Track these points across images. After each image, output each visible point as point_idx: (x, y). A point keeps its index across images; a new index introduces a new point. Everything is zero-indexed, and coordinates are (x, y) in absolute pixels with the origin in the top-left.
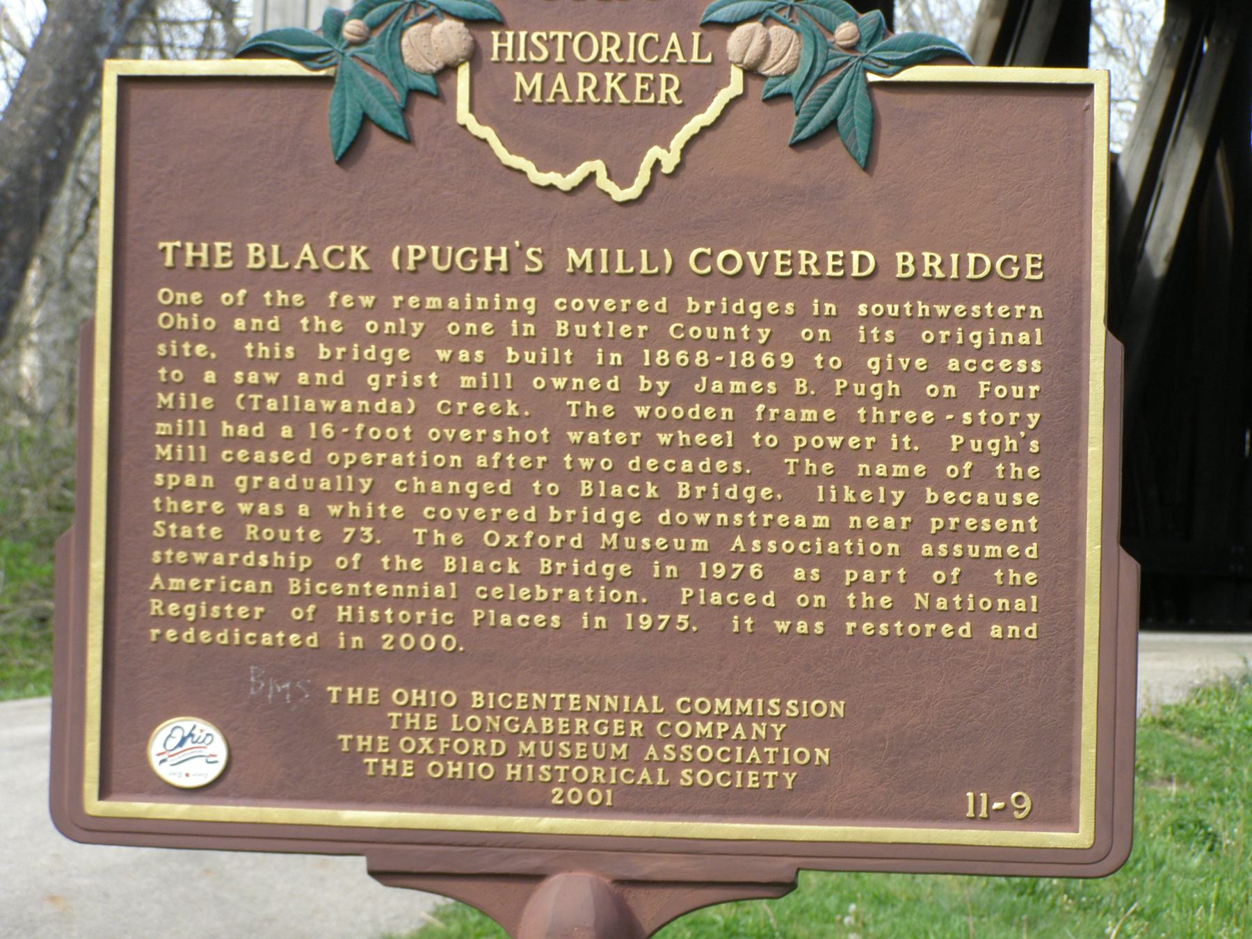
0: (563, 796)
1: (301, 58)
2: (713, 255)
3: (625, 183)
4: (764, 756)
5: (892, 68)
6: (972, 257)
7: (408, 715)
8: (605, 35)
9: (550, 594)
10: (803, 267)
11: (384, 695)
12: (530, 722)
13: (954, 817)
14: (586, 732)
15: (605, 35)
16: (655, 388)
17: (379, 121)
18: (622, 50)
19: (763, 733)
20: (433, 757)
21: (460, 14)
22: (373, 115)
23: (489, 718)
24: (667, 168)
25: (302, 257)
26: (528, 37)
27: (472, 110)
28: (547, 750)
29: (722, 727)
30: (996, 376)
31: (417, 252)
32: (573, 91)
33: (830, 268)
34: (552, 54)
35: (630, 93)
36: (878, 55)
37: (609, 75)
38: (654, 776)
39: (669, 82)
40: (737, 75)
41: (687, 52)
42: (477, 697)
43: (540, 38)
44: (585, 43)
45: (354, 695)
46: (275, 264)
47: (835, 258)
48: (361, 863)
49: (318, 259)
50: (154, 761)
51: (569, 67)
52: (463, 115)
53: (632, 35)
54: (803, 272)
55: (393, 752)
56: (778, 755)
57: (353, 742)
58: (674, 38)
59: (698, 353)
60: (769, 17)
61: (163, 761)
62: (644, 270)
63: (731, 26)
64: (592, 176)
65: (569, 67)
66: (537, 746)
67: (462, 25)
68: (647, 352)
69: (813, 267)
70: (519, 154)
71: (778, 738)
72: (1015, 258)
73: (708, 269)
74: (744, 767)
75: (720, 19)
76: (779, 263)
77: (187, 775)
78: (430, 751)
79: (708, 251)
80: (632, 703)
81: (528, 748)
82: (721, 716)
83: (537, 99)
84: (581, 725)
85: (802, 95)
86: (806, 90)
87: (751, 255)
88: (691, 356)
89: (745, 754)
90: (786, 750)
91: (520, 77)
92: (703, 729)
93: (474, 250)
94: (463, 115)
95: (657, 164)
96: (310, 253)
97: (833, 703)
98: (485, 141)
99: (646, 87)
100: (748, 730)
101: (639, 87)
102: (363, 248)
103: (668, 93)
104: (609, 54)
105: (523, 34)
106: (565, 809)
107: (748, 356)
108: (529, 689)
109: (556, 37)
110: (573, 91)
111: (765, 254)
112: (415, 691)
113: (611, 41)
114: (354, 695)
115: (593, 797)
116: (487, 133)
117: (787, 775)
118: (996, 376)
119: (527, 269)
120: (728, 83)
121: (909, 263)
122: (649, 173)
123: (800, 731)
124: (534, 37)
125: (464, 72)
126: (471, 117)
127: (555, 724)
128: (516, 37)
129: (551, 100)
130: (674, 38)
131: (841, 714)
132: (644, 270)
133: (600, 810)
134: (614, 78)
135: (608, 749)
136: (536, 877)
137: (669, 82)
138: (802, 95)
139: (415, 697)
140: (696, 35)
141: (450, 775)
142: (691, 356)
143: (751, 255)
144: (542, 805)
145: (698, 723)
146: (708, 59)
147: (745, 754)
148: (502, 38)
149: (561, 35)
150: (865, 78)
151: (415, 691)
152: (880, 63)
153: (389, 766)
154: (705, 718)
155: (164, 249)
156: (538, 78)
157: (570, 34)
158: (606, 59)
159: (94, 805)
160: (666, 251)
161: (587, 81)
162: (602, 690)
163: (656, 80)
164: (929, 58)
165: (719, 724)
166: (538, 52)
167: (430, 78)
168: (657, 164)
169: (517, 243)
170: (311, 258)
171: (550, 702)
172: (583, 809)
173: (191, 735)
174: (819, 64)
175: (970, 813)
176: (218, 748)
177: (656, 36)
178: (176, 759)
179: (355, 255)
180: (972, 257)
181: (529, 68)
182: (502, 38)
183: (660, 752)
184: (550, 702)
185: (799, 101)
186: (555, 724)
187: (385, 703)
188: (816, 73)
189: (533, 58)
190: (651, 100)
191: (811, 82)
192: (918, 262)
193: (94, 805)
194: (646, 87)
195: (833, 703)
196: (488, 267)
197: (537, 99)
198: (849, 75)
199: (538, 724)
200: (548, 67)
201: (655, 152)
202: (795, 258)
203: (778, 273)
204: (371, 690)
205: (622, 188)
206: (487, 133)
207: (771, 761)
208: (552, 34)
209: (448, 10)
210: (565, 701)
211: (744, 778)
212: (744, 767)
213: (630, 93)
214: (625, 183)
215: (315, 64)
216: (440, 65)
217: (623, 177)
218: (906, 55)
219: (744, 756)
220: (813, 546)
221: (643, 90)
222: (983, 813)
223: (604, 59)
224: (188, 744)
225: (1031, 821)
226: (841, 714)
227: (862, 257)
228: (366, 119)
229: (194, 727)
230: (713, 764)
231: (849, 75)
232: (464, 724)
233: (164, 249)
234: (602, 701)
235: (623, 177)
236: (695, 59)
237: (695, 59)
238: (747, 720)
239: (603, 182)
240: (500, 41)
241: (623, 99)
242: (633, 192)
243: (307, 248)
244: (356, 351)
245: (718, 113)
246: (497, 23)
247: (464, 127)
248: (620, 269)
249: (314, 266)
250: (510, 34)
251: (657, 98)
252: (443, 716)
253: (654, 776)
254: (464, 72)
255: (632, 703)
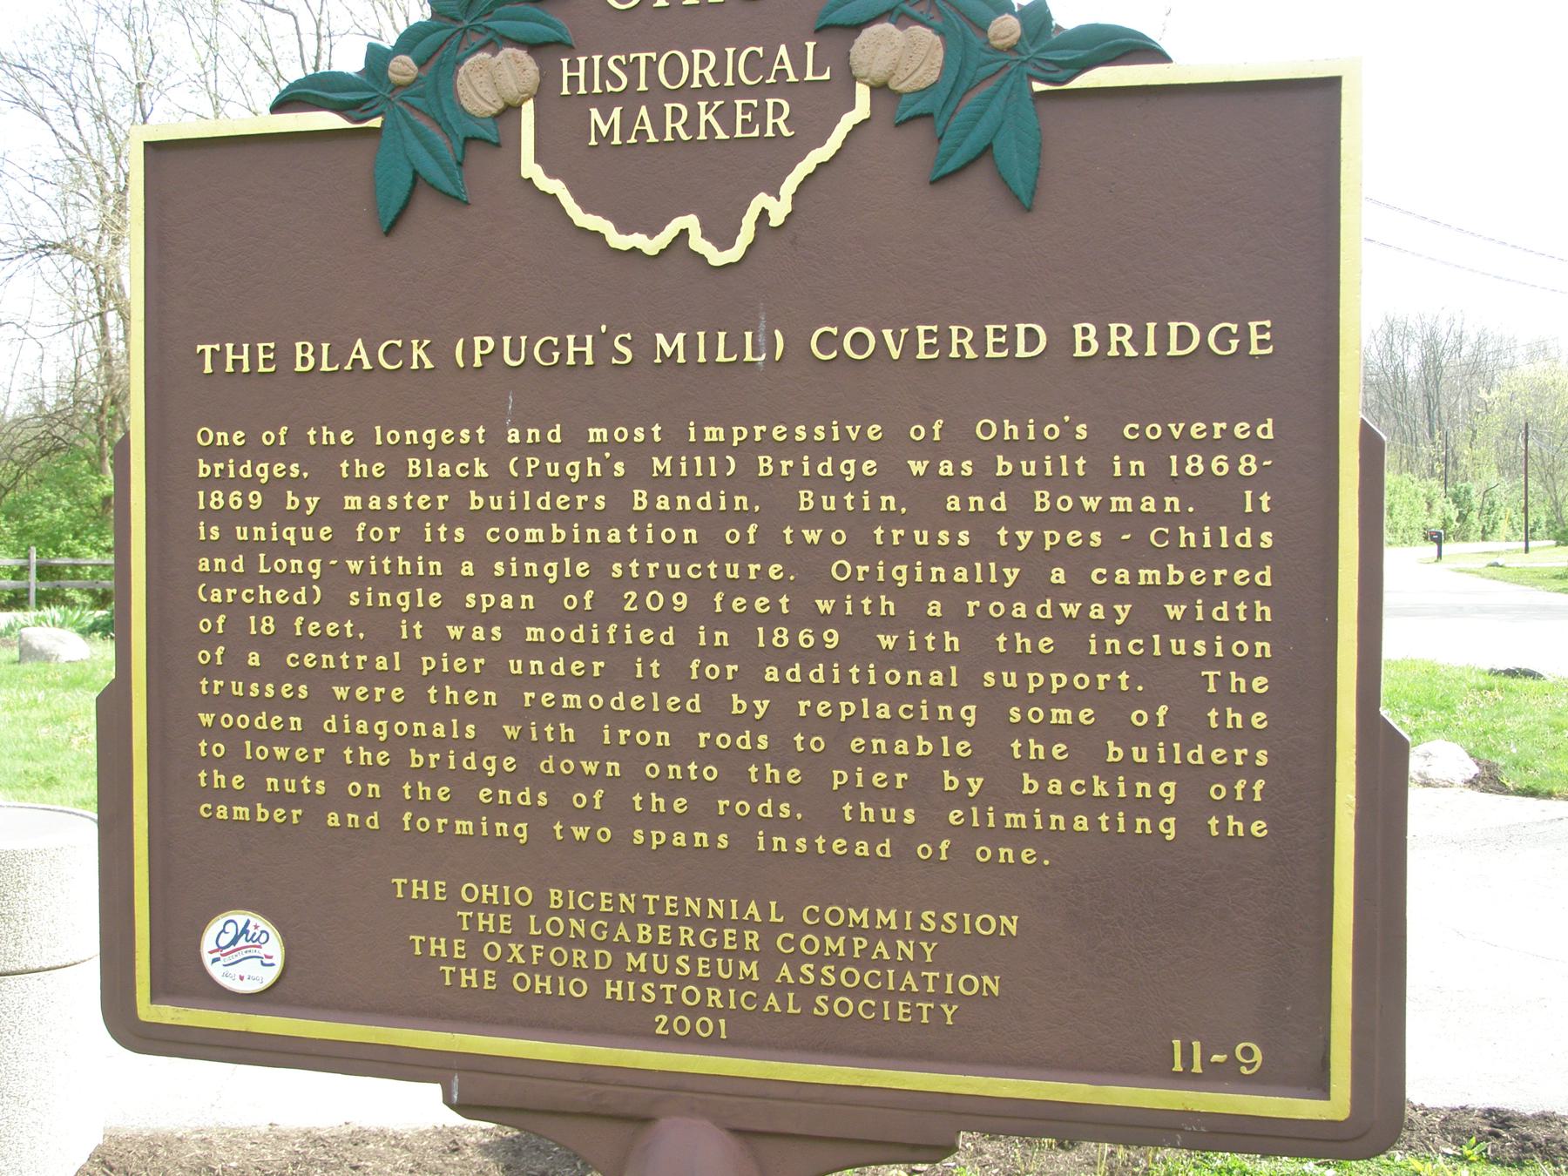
0: (668, 1025)
1: (340, 108)
2: (841, 334)
5: (1062, 74)
6: (1173, 326)
7: (480, 915)
8: (697, 53)
9: (427, 760)
11: (452, 891)
12: (622, 930)
13: (1159, 1072)
14: (692, 944)
16: (304, 506)
17: (430, 180)
18: (719, 72)
19: (910, 954)
20: (521, 967)
21: (521, 38)
22: (423, 173)
23: (573, 922)
24: (776, 220)
25: (354, 356)
26: (603, 62)
27: (537, 160)
28: (661, 966)
29: (860, 943)
30: (820, 485)
31: (484, 345)
34: (633, 81)
35: (729, 128)
36: (1042, 56)
37: (703, 105)
38: (783, 1002)
39: (778, 109)
40: (863, 93)
41: (800, 69)
42: (555, 895)
43: (617, 62)
44: (673, 67)
45: (420, 889)
46: (325, 368)
47: (928, 334)
48: (435, 1090)
49: (880, 339)
50: (207, 959)
51: (656, 97)
52: (530, 168)
53: (730, 51)
54: (954, 354)
55: (474, 959)
57: (425, 945)
58: (783, 51)
60: (903, 14)
61: (215, 960)
64: (684, 233)
66: (649, 961)
70: (595, 213)
71: (929, 960)
72: (1234, 328)
73: (834, 354)
74: (895, 995)
75: (840, 21)
76: (922, 341)
77: (242, 978)
78: (521, 960)
80: (742, 908)
83: (617, 141)
85: (945, 116)
86: (950, 108)
87: (887, 333)
88: (1234, 464)
89: (898, 980)
90: (949, 976)
91: (595, 114)
92: (836, 945)
93: (555, 341)
94: (530, 168)
95: (764, 213)
96: (362, 351)
97: (1004, 919)
99: (749, 117)
100: (892, 949)
101: (740, 117)
102: (426, 342)
103: (778, 123)
105: (597, 58)
106: (672, 1042)
107: (1195, 460)
108: (616, 887)
111: (904, 331)
112: (485, 887)
113: (704, 60)
114: (420, 889)
115: (705, 1026)
116: (556, 187)
117: (945, 1007)
118: (820, 485)
119: (614, 361)
120: (852, 107)
121: (1091, 337)
123: (962, 952)
124: (611, 64)
127: (655, 932)
128: (589, 63)
129: (633, 140)
130: (783, 51)
131: (1014, 932)
133: (713, 1045)
134: (708, 109)
136: (646, 1120)
137: (778, 109)
138: (945, 116)
139: (485, 894)
140: (810, 45)
141: (538, 991)
143: (887, 333)
144: (644, 1036)
146: (827, 76)
147: (898, 980)
148: (573, 66)
149: (643, 56)
151: (485, 887)
153: (468, 978)
154: (835, 933)
155: (203, 351)
156: (616, 113)
157: (653, 55)
158: (705, 84)
160: (777, 333)
161: (676, 114)
164: (1115, 54)
165: (856, 940)
166: (616, 81)
167: (491, 123)
168: (764, 213)
169: (603, 328)
170: (363, 356)
171: (641, 904)
172: (692, 1043)
173: (245, 931)
174: (969, 74)
175: (1178, 1067)
176: (275, 948)
177: (760, 50)
178: (228, 960)
179: (417, 352)
180: (1174, 326)
181: (605, 102)
182: (573, 66)
183: (796, 973)
184: (641, 904)
186: (655, 932)
188: (965, 84)
189: (610, 88)
190: (756, 133)
191: (956, 98)
192: (1103, 338)
195: (1004, 919)
196: (571, 361)
197: (617, 141)
199: (633, 933)
200: (629, 101)
201: (761, 200)
203: (922, 355)
205: (721, 249)
206: (556, 187)
207: (931, 989)
208: (632, 56)
209: (509, 34)
211: (894, 1010)
212: (895, 995)
213: (729, 128)
217: (723, 237)
218: (1080, 54)
219: (898, 983)
222: (1197, 1069)
223: (696, 84)
224: (242, 942)
225: (1262, 1082)
226: (1014, 932)
227: (1028, 331)
229: (248, 923)
230: (859, 992)
231: (1007, 86)
233: (203, 351)
234: (705, 906)
235: (723, 237)
236: (809, 76)
237: (809, 76)
239: (698, 243)
240: (569, 70)
241: (721, 135)
242: (734, 254)
243: (359, 344)
246: (562, 46)
249: (367, 366)
250: (582, 60)
251: (763, 129)
253: (783, 1002)
255: (742, 908)
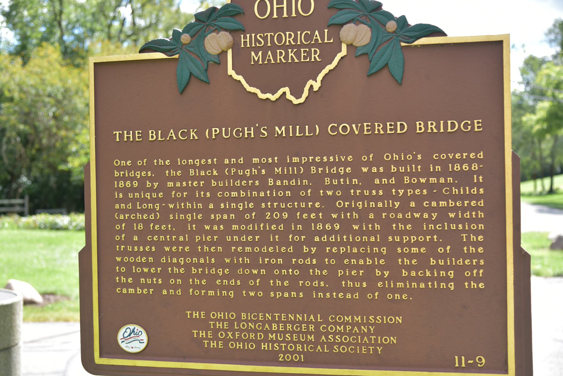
3: (298, 97)
4: (370, 340)
8: (288, 33)
10: (429, 129)
11: (207, 315)
15: (288, 33)
18: (295, 40)
20: (232, 340)
22: (194, 73)
24: (316, 88)
25: (170, 135)
26: (255, 36)
29: (349, 328)
31: (216, 131)
32: (275, 59)
33: (365, 130)
34: (266, 42)
37: (290, 50)
38: (323, 348)
39: (315, 52)
40: (344, 47)
41: (323, 39)
42: (243, 315)
43: (260, 36)
44: (280, 38)
45: (196, 315)
50: (120, 341)
53: (299, 33)
55: (215, 338)
56: (376, 340)
57: (198, 334)
58: (317, 33)
59: (473, 165)
61: (122, 342)
62: (307, 134)
63: (342, 25)
64: (284, 93)
65: (274, 48)
66: (276, 336)
67: (227, 33)
68: (450, 165)
69: (434, 129)
72: (469, 122)
74: (361, 345)
75: (336, 23)
77: (132, 348)
79: (336, 125)
81: (272, 336)
82: (348, 323)
83: (261, 63)
84: (289, 327)
86: (374, 51)
87: (354, 126)
88: (470, 166)
89: (362, 339)
91: (253, 53)
92: (341, 328)
95: (311, 86)
98: (239, 81)
100: (360, 329)
101: (302, 55)
103: (315, 56)
104: (289, 41)
105: (253, 35)
106: (285, 364)
107: (457, 166)
109: (267, 35)
110: (275, 59)
111: (359, 125)
114: (196, 315)
115: (296, 358)
116: (240, 78)
117: (378, 348)
120: (341, 51)
121: (422, 126)
122: (308, 92)
125: (230, 53)
126: (234, 72)
128: (251, 37)
130: (317, 33)
132: (307, 134)
135: (306, 337)
137: (315, 52)
138: (372, 54)
140: (326, 31)
142: (470, 166)
143: (354, 126)
145: (338, 327)
147: (362, 339)
149: (269, 34)
150: (400, 44)
152: (407, 38)
153: (213, 344)
157: (273, 34)
159: (98, 360)
160: (317, 126)
161: (281, 54)
162: (295, 313)
163: (311, 51)
166: (260, 43)
168: (311, 86)
169: (257, 125)
174: (379, 40)
177: (309, 32)
180: (449, 122)
182: (245, 37)
183: (327, 338)
184: (274, 317)
185: (371, 57)
187: (208, 318)
189: (258, 45)
190: (308, 60)
191: (375, 48)
193: (98, 360)
194: (306, 54)
195: (397, 318)
198: (392, 44)
200: (265, 49)
202: (373, 127)
203: (365, 133)
204: (202, 313)
205: (297, 99)
206: (240, 78)
208: (265, 34)
210: (280, 317)
213: (299, 58)
214: (298, 97)
215: (170, 53)
216: (220, 51)
217: (297, 94)
218: (417, 33)
219: (362, 341)
220: (367, 250)
221: (304, 56)
223: (287, 44)
227: (401, 124)
228: (191, 74)
232: (240, 327)
235: (297, 94)
236: (326, 41)
237: (326, 41)
238: (358, 325)
239: (289, 96)
241: (296, 61)
242: (302, 100)
244: (127, 173)
245: (336, 64)
246: (243, 31)
247: (231, 76)
248: (298, 134)
251: (311, 59)
252: (231, 323)
253: (323, 348)
254: (230, 53)
255: (308, 317)
